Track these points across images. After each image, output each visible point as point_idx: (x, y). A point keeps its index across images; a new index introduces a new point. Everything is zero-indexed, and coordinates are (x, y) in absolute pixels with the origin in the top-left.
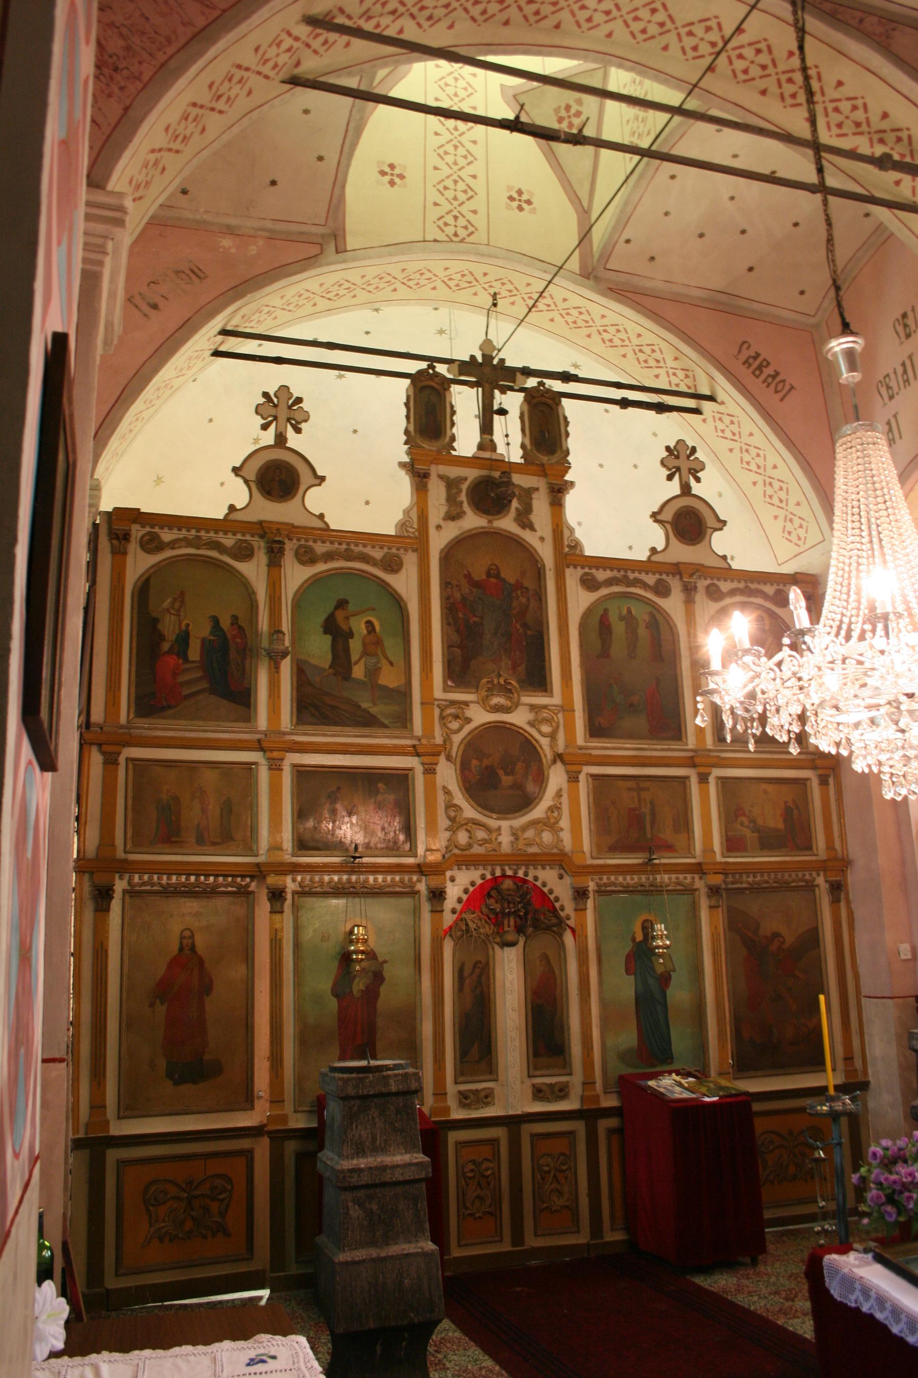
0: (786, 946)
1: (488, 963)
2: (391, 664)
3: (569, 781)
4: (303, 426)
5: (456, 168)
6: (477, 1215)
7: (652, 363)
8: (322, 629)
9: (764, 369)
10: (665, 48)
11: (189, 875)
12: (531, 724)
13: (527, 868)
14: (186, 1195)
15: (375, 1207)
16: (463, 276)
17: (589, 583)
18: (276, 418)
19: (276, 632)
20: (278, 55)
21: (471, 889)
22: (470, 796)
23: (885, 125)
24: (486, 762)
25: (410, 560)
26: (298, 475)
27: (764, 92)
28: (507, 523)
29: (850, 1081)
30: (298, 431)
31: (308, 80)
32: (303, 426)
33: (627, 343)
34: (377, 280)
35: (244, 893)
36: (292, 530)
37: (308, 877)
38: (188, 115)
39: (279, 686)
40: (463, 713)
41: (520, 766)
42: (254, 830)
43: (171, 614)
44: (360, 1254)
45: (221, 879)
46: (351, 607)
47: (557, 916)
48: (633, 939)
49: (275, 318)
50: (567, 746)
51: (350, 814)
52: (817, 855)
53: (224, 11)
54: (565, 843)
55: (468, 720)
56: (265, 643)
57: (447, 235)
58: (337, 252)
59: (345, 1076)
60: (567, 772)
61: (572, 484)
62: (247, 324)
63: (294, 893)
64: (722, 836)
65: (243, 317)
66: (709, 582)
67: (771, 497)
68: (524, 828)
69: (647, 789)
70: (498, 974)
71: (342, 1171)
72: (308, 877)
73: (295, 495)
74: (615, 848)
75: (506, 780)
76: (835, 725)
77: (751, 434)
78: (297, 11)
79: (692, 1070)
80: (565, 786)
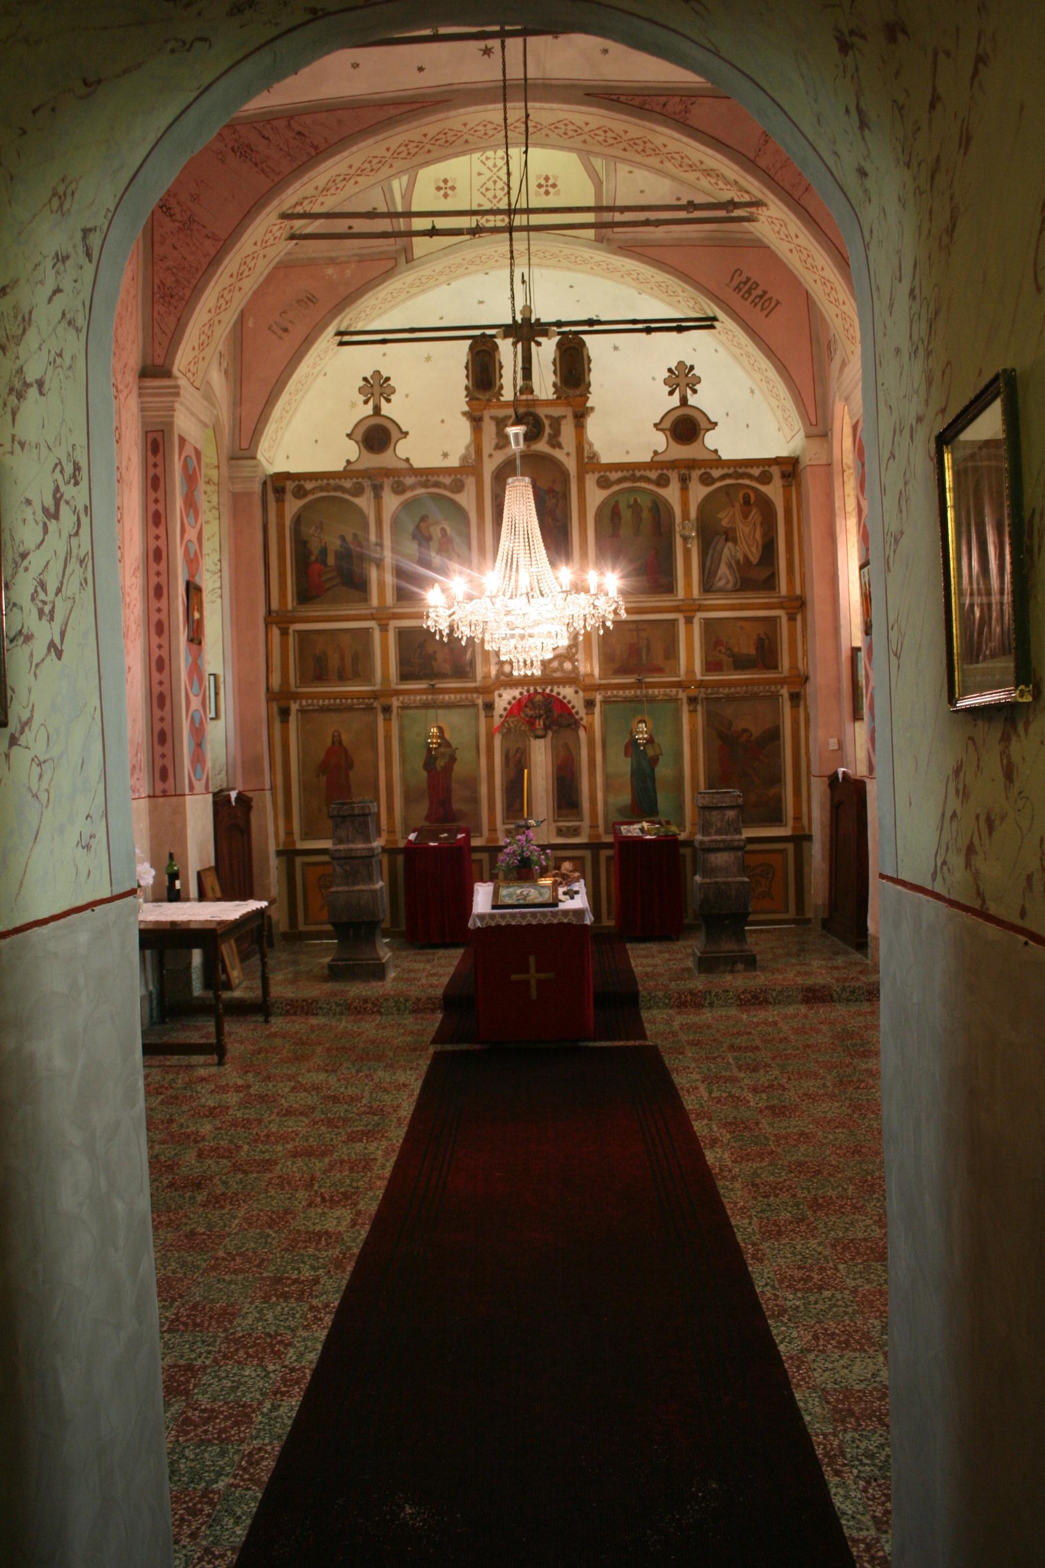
0: (753, 738)
4: (392, 397)
5: (495, 170)
11: (335, 699)
15: (348, 868)
17: (603, 483)
18: (373, 394)
25: (470, 482)
30: (388, 401)
32: (392, 397)
35: (370, 709)
36: (388, 472)
42: (372, 670)
58: (407, 262)
61: (592, 409)
63: (399, 707)
66: (703, 471)
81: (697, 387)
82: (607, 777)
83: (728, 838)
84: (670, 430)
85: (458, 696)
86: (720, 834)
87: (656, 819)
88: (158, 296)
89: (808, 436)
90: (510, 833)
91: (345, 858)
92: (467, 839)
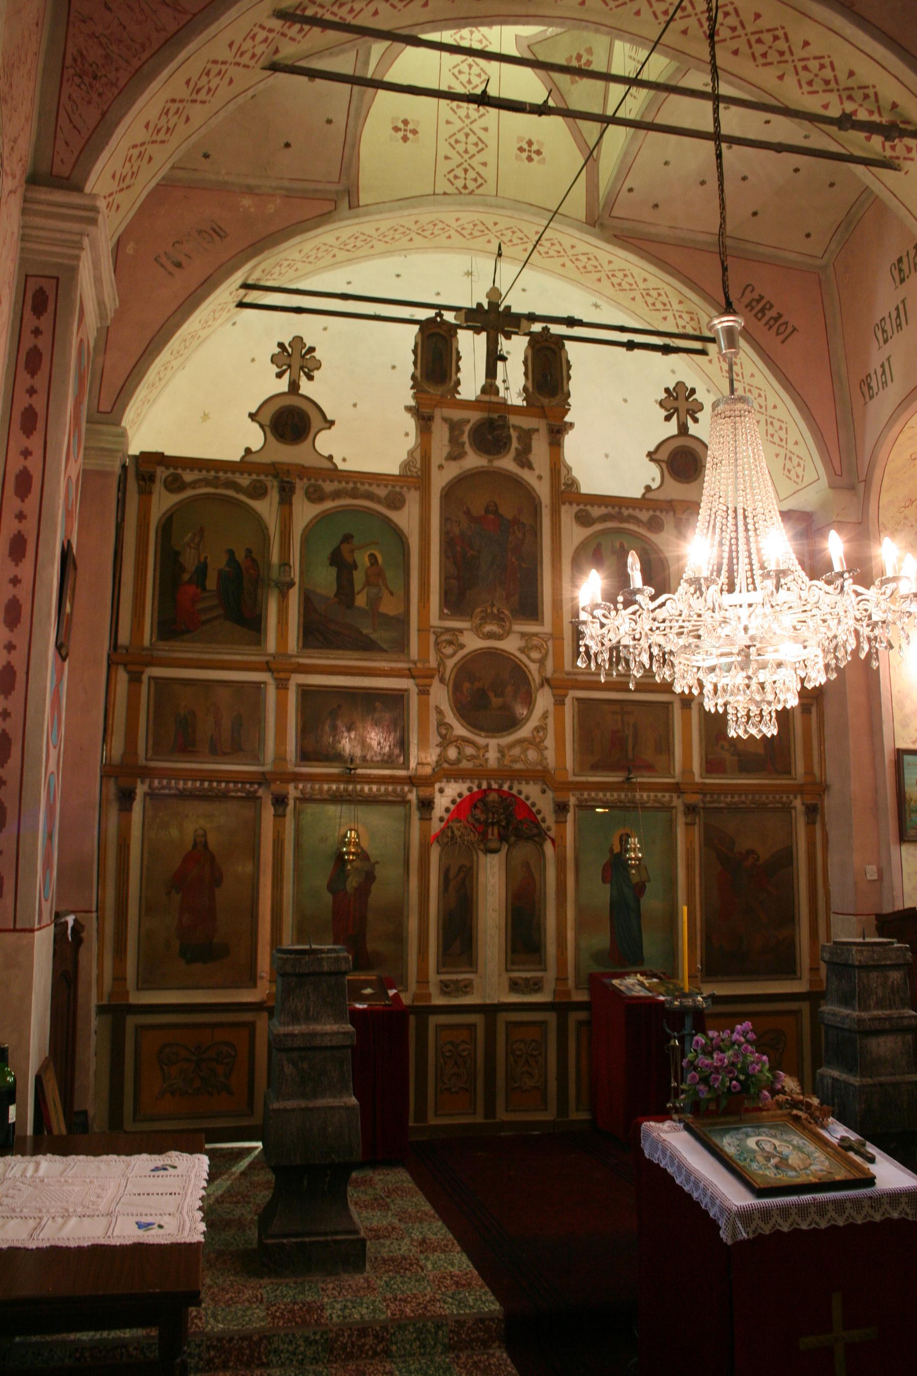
1: (471, 868)
2: (392, 594)
3: (555, 704)
5: (467, 121)
6: (453, 1090)
7: (659, 306)
8: (328, 562)
9: (767, 312)
10: (638, 13)
11: (202, 781)
12: (521, 650)
13: (512, 783)
14: (194, 1058)
15: (305, 1066)
16: (475, 225)
17: (583, 519)
19: (285, 564)
20: (254, 47)
21: (458, 800)
22: (462, 716)
23: (851, 83)
25: (413, 498)
26: (309, 419)
27: (736, 52)
28: (507, 463)
29: (815, 990)
30: (310, 378)
31: (287, 66)
32: (316, 374)
33: (634, 286)
34: (392, 232)
36: (303, 471)
37: (309, 786)
38: (168, 110)
39: (287, 613)
40: (458, 640)
41: (509, 690)
42: (262, 741)
43: (191, 547)
44: (290, 1104)
45: (231, 785)
46: (356, 541)
47: (537, 825)
48: (611, 850)
49: (297, 270)
50: (554, 672)
51: (349, 730)
52: (795, 779)
53: (195, 15)
54: (549, 761)
55: (462, 646)
56: (274, 574)
57: (457, 188)
58: (350, 208)
59: (285, 956)
60: (554, 695)
61: (571, 425)
62: (268, 277)
63: (296, 799)
64: (701, 759)
65: (263, 271)
67: (772, 436)
68: (511, 746)
70: (481, 878)
71: (278, 1035)
72: (309, 786)
73: (306, 438)
74: (595, 768)
75: (496, 701)
76: (695, 670)
77: (752, 375)
78: (267, 6)
79: (655, 971)
80: (551, 708)
81: (698, 415)
83: (894, 1013)
84: (667, 462)
86: (883, 1008)
88: (71, 71)
89: (832, 486)
90: (447, 986)
91: (299, 1049)
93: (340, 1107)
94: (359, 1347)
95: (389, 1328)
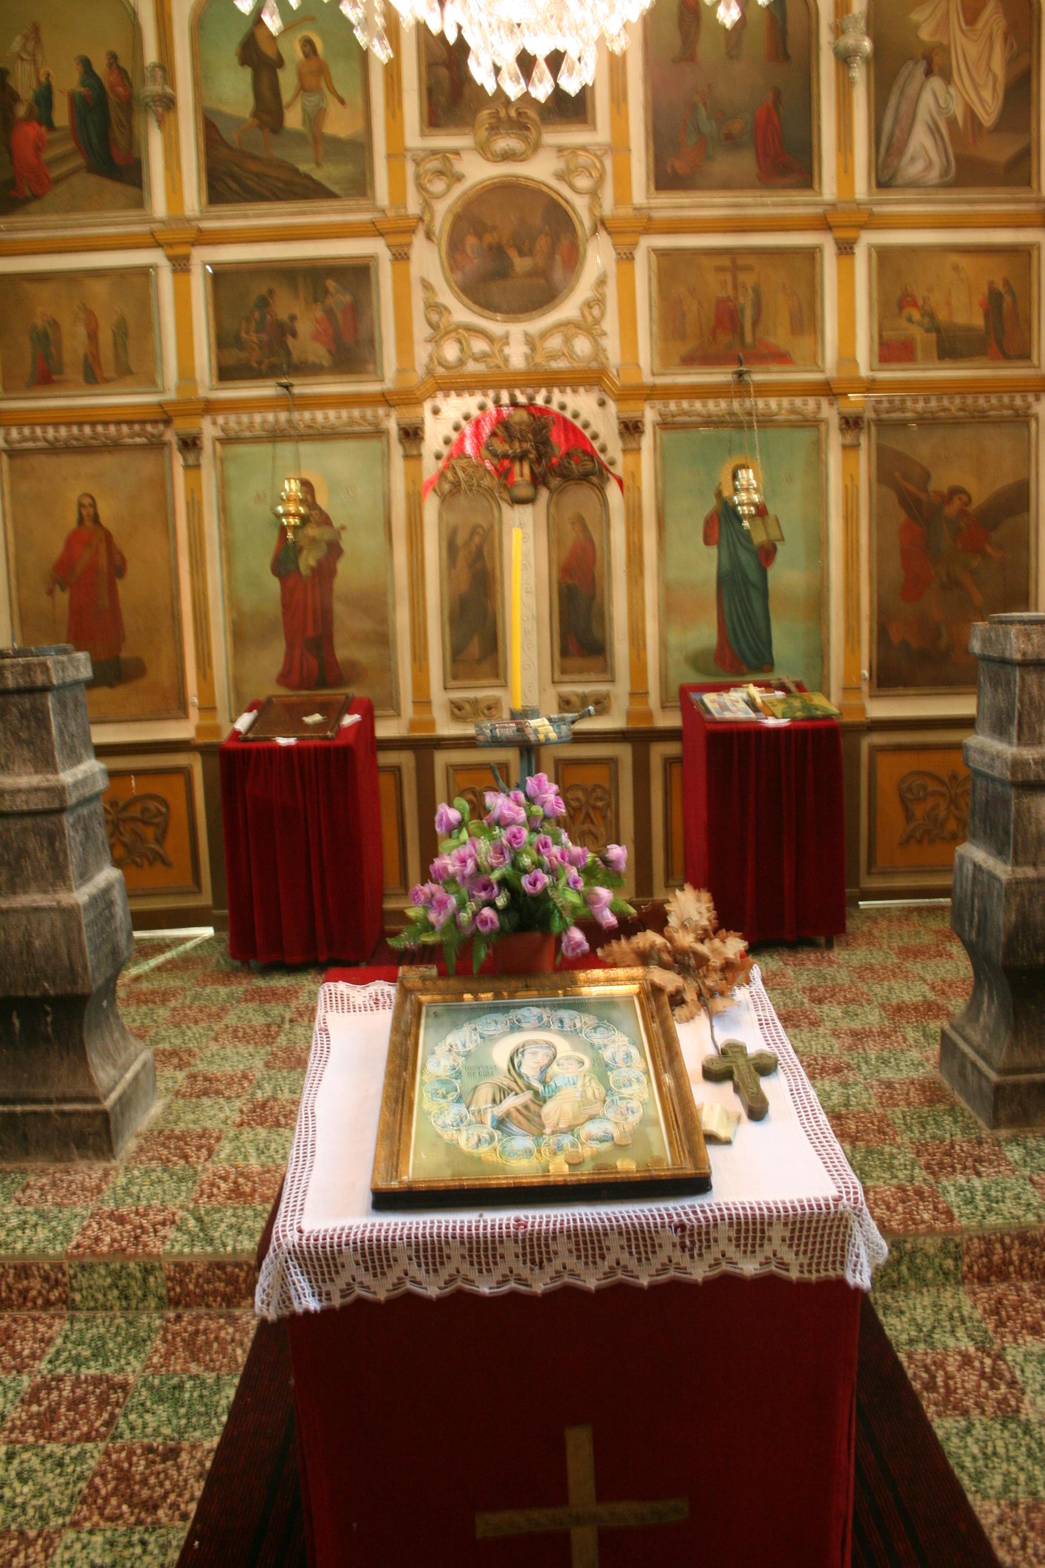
2: (342, 102)
8: (235, 60)
12: (560, 176)
13: (550, 392)
24: (489, 239)
35: (157, 445)
41: (542, 244)
54: (610, 355)
55: (459, 178)
68: (545, 335)
69: (749, 268)
74: (689, 361)
75: (521, 264)
80: (612, 269)
82: (667, 589)
85: (344, 413)
87: (772, 678)
90: (460, 709)
92: (367, 725)
93: (51, 909)
94: (20, 1292)
95: (66, 1267)
